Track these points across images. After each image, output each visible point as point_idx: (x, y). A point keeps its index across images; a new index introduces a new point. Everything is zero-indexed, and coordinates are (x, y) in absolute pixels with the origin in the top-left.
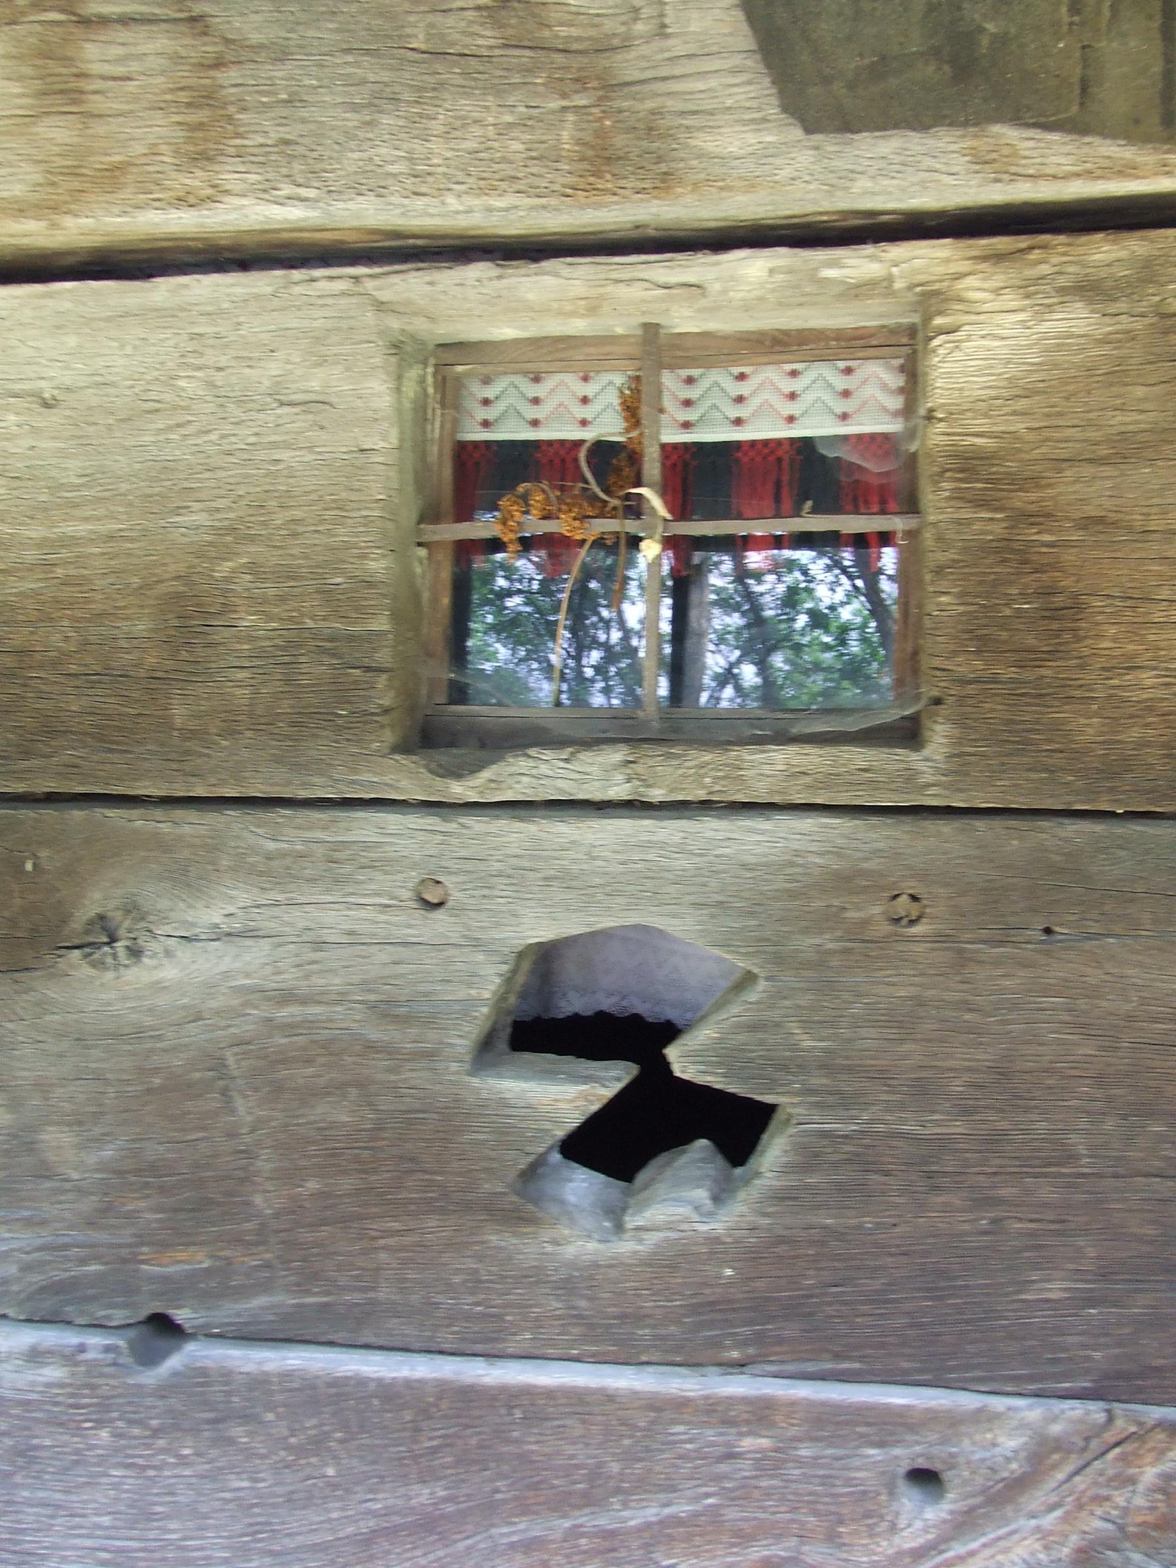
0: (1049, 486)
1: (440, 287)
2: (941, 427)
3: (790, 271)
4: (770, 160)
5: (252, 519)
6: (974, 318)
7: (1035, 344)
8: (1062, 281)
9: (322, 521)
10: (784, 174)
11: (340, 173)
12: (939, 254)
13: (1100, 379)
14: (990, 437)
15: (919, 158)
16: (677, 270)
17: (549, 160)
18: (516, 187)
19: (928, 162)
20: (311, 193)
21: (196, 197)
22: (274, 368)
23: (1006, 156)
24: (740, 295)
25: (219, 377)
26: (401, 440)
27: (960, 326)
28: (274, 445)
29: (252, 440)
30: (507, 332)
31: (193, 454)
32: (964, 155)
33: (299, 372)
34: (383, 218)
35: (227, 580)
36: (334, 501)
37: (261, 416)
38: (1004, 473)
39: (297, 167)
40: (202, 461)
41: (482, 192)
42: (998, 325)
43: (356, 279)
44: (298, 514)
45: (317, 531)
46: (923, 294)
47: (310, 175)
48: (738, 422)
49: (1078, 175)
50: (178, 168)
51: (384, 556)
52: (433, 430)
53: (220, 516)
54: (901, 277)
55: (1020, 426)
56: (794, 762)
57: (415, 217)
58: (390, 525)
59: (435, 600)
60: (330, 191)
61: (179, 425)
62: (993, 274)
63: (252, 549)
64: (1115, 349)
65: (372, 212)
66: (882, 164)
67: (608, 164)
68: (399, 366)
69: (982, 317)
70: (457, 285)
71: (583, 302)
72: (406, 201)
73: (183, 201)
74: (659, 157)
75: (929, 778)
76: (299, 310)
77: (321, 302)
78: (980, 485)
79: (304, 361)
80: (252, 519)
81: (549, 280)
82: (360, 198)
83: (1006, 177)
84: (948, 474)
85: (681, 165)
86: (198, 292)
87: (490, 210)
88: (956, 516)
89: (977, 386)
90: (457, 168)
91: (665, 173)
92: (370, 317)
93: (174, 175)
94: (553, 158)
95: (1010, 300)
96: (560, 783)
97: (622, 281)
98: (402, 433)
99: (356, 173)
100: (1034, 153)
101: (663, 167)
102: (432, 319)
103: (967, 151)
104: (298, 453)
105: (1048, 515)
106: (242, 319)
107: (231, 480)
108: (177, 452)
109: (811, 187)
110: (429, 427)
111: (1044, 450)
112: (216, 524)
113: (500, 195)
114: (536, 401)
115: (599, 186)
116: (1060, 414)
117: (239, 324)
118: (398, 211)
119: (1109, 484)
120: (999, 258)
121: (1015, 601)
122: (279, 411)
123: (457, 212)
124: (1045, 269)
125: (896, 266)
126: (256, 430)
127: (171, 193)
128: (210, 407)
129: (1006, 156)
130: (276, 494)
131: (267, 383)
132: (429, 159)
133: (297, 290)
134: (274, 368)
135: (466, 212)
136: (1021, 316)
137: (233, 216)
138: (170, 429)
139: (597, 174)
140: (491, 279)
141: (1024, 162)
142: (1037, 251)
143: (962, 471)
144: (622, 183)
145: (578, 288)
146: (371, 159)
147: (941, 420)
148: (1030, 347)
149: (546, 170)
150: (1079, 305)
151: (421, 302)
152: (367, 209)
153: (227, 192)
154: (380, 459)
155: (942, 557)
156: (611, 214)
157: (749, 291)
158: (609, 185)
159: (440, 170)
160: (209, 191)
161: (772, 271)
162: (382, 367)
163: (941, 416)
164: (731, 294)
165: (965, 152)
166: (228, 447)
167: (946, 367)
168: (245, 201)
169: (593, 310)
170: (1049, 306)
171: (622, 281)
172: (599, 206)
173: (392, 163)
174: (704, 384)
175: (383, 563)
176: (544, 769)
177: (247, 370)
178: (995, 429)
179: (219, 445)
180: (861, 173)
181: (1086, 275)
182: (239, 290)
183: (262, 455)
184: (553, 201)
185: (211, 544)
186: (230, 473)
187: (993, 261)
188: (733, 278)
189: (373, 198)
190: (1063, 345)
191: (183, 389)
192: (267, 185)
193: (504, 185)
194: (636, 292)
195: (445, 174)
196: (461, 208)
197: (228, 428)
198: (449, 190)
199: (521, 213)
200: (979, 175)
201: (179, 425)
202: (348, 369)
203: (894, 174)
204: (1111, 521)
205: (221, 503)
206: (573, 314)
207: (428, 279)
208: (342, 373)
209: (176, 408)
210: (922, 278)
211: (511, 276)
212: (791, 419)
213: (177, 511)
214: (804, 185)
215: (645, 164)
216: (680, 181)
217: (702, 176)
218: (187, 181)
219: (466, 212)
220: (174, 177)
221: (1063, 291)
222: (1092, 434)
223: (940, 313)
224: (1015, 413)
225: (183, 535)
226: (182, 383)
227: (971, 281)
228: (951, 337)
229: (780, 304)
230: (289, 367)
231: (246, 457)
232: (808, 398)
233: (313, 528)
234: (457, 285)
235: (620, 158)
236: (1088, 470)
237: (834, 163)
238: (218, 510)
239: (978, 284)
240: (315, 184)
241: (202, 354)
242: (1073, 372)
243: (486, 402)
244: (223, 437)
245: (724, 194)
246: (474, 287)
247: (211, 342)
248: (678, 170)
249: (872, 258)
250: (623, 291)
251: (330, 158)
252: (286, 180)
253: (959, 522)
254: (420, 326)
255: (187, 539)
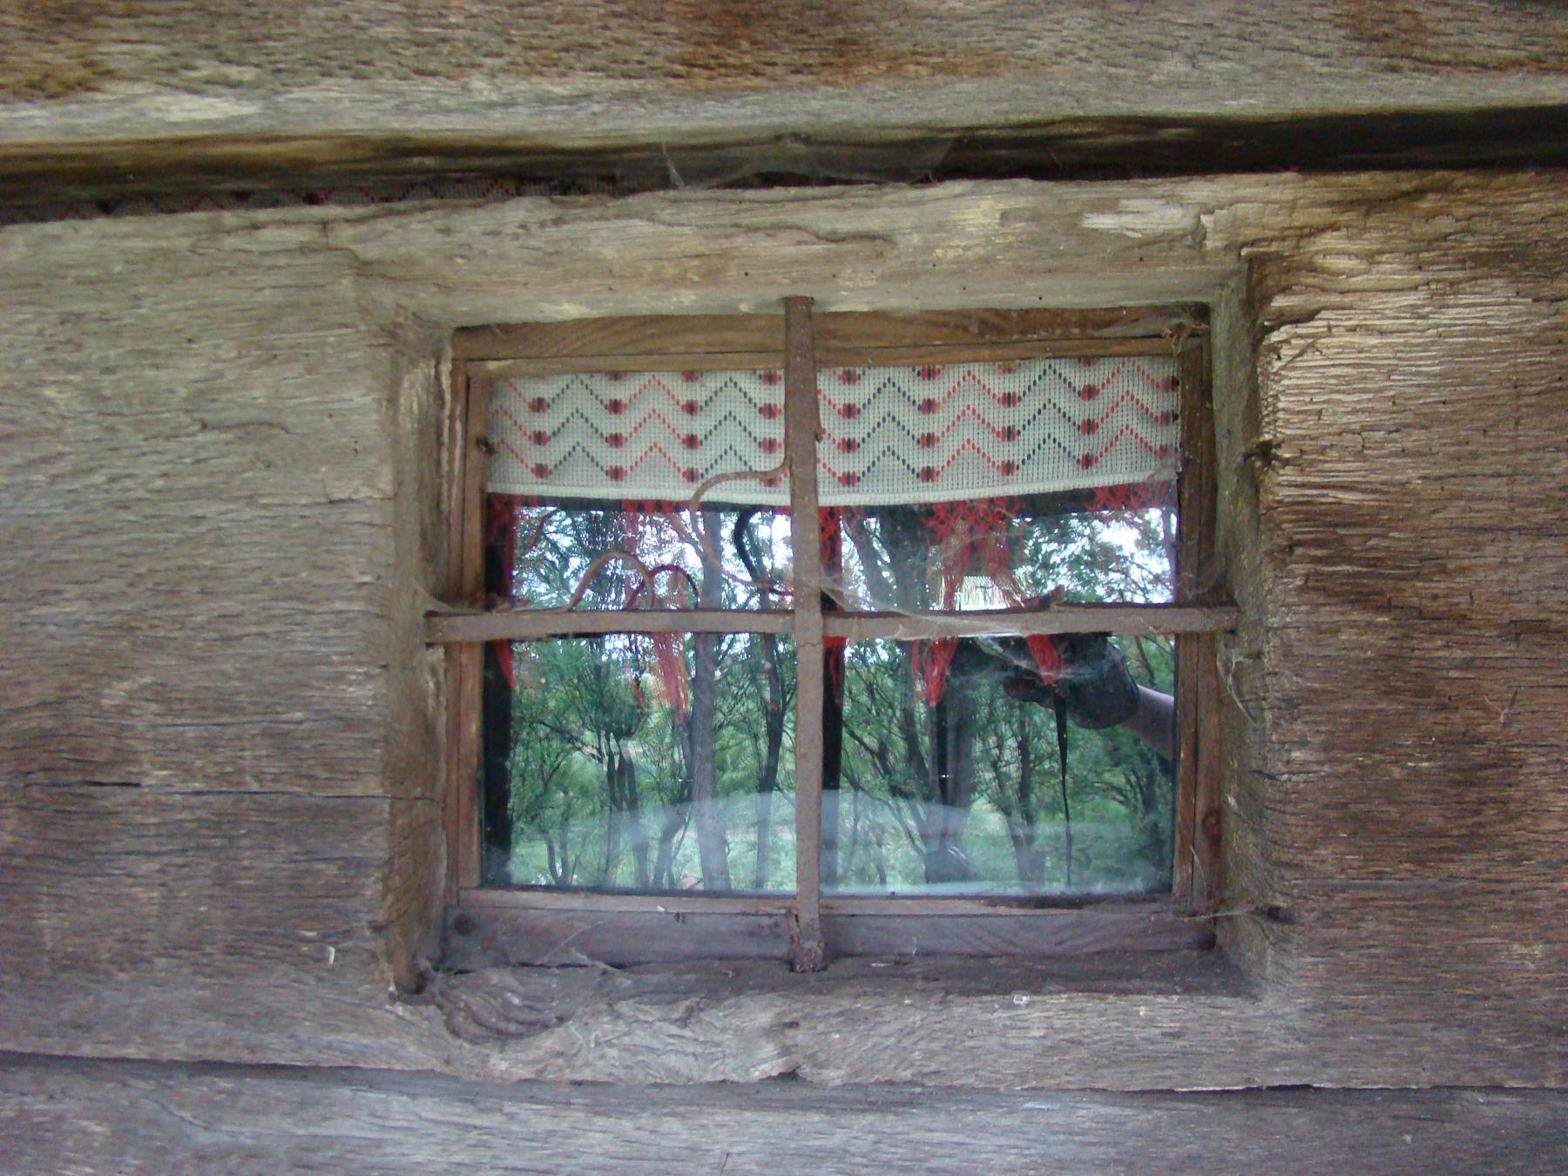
0: (1462, 571)
1: (460, 238)
2: (1288, 475)
3: (1035, 217)
4: (1020, 22)
5: (159, 613)
6: (1336, 299)
7: (1433, 343)
8: (1470, 244)
9: (271, 619)
10: (1043, 45)
11: (294, 40)
12: (1276, 196)
13: (1533, 400)
14: (1364, 491)
15: (1266, 28)
16: (851, 212)
17: (646, 18)
18: (588, 61)
19: (1281, 34)
20: (248, 74)
21: (60, 83)
22: (193, 369)
23: (1405, 31)
24: (952, 254)
25: (106, 384)
26: (399, 483)
27: (1317, 311)
28: (195, 494)
29: (159, 483)
30: (570, 310)
31: (67, 507)
32: (1338, 26)
33: (231, 375)
34: (367, 115)
35: (122, 710)
36: (288, 585)
37: (173, 445)
38: (1388, 549)
39: (225, 31)
40: (81, 519)
41: (531, 70)
42: (1374, 312)
43: (325, 225)
44: (230, 606)
45: (261, 635)
46: (1251, 260)
47: (244, 45)
48: (928, 474)
49: (1518, 64)
50: (30, 35)
51: (369, 677)
52: (451, 461)
53: (109, 607)
54: (1215, 232)
55: (1411, 474)
56: (1058, 1024)
57: (420, 114)
58: (380, 626)
59: (456, 727)
60: (279, 71)
61: (45, 460)
62: (1365, 229)
63: (160, 661)
64: (1553, 353)
65: (347, 104)
66: (1207, 35)
67: (746, 25)
68: (395, 364)
69: (1348, 299)
70: (486, 234)
71: (696, 263)
72: (404, 86)
73: (41, 88)
74: (829, 15)
75: (1279, 1046)
76: (232, 273)
77: (268, 261)
78: (1346, 568)
79: (240, 357)
80: (159, 613)
81: (639, 227)
82: (328, 81)
83: (1406, 64)
84: (1299, 551)
85: (870, 28)
86: (73, 246)
87: (544, 100)
88: (1313, 618)
89: (1345, 410)
90: (489, 31)
91: (842, 42)
92: (346, 287)
93: (23, 46)
94: (652, 15)
95: (1391, 270)
96: (672, 1060)
97: (757, 229)
98: (398, 472)
99: (321, 40)
100: (1450, 28)
101: (840, 32)
102: (445, 288)
103: (1344, 20)
104: (232, 506)
105: (1463, 619)
106: (142, 289)
107: (126, 549)
108: (44, 503)
109: (1090, 69)
110: (445, 456)
111: (1452, 512)
112: (101, 618)
113: (562, 75)
114: (616, 440)
115: (731, 60)
116: (1474, 455)
117: (137, 298)
118: (393, 102)
119: (1551, 567)
120: (1370, 205)
121: (1410, 756)
122: (200, 438)
123: (491, 105)
124: (1444, 224)
125: (1211, 212)
126: (164, 468)
127: (20, 77)
128: (93, 432)
129: (1405, 31)
130: (196, 573)
131: (183, 392)
132: (441, 15)
133: (230, 242)
134: (193, 369)
135: (505, 105)
136: (1411, 299)
137: (118, 114)
138: (30, 464)
139: (727, 40)
140: (542, 224)
141: (1432, 41)
142: (1431, 196)
143: (1319, 544)
144: (772, 55)
145: (688, 239)
146: (346, 18)
147: (1286, 462)
148: (1425, 347)
149: (639, 35)
150: (1498, 283)
151: (429, 261)
152: (338, 100)
153: (109, 74)
154: (365, 517)
155: (1288, 683)
156: (748, 111)
157: (966, 249)
158: (747, 59)
159: (459, 34)
160: (81, 73)
161: (1004, 216)
162: (367, 367)
163: (1287, 456)
164: (939, 252)
165: (1338, 20)
166: (118, 496)
167: (1292, 380)
168: (138, 88)
169: (712, 275)
170: (1452, 284)
171: (757, 229)
172: (726, 95)
173: (381, 23)
174: (871, 417)
175: (370, 689)
176: (641, 1037)
177: (151, 373)
178: (1373, 478)
179: (107, 491)
180: (1172, 49)
181: (1509, 236)
182: (138, 244)
183: (171, 509)
184: (652, 85)
185: (95, 652)
186: (125, 537)
187: (1363, 209)
188: (941, 227)
189: (349, 81)
190: (1477, 344)
191: (51, 402)
192: (175, 62)
193: (569, 58)
194: (784, 247)
195: (468, 41)
196: (495, 97)
197: (119, 465)
198: (474, 66)
199: (596, 108)
200: (1365, 59)
201: (45, 460)
202: (309, 371)
203: (1226, 53)
204: (1553, 626)
205: (112, 585)
206: (681, 281)
207: (439, 223)
208: (301, 376)
209: (37, 433)
210: (1250, 233)
211: (578, 219)
212: (1008, 468)
213: (42, 597)
214: (1077, 64)
215: (806, 25)
216: (869, 56)
217: (906, 47)
218: (47, 57)
219: (505, 105)
220: (24, 49)
221: (1478, 259)
222: (1523, 489)
223: (1285, 290)
224: (1403, 453)
225: (51, 636)
226: (50, 393)
227: (1328, 240)
228: (1302, 329)
229: (1018, 269)
230: (219, 366)
231: (149, 511)
232: (1031, 437)
233: (254, 629)
234: (486, 234)
235: (763, 16)
236: (1520, 547)
237: (1126, 32)
238: (105, 597)
239: (1341, 245)
240: (254, 59)
241: (79, 347)
242: (1491, 389)
243: (539, 438)
244: (113, 480)
245: (939, 78)
246: (516, 237)
247: (93, 326)
248: (862, 36)
249: (1171, 200)
250: (764, 246)
251: (280, 17)
252: (206, 53)
253: (1318, 629)
254: (429, 300)
255: (58, 644)
